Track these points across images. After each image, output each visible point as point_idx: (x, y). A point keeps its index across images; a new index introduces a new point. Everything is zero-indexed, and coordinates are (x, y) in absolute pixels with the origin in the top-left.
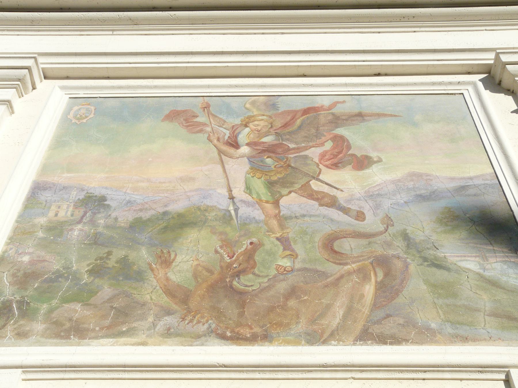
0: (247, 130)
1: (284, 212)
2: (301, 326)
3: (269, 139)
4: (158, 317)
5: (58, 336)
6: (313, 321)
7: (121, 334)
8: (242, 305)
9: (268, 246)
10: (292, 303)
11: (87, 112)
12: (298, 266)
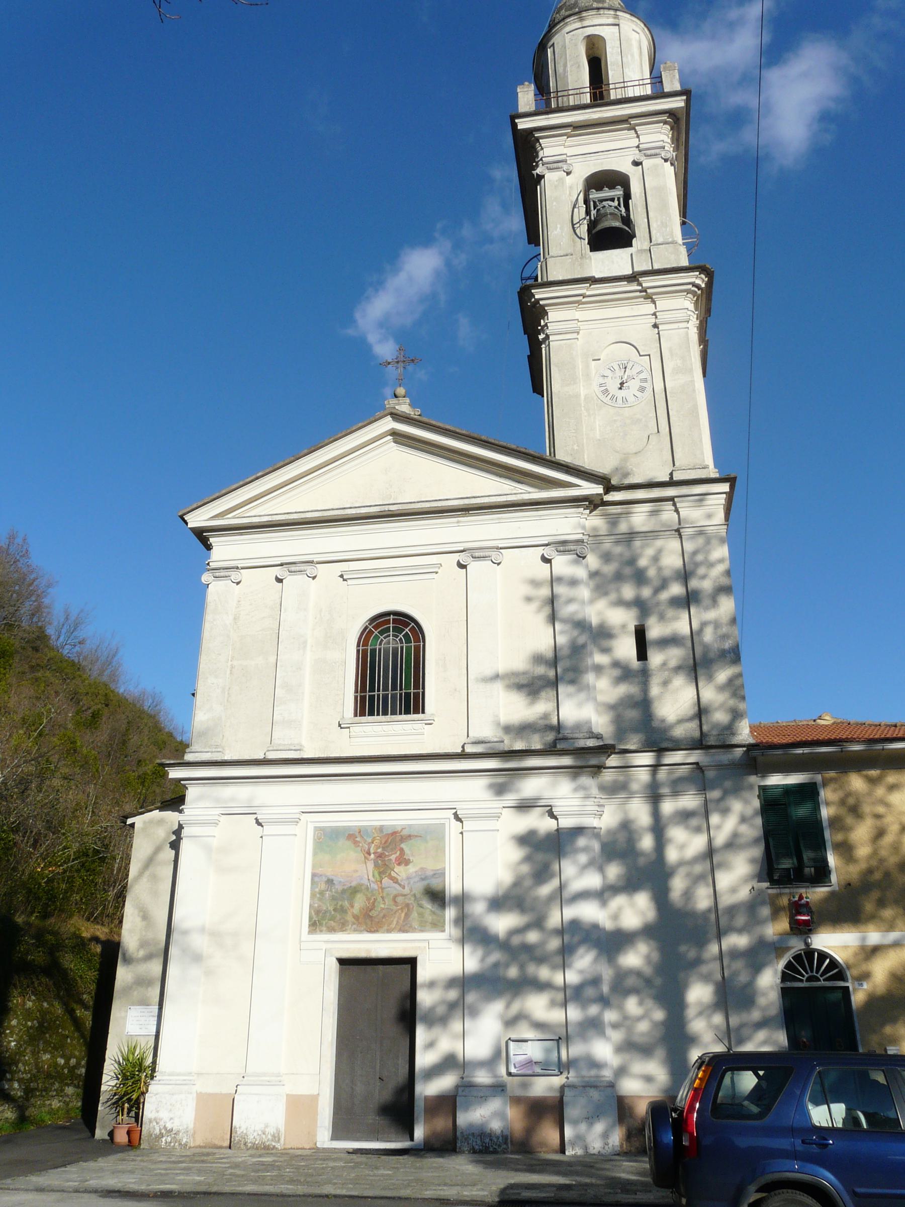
0: (373, 845)
1: (383, 886)
2: (385, 928)
3: (380, 850)
4: (352, 926)
5: (329, 931)
6: (388, 926)
7: (343, 931)
8: (372, 921)
9: (378, 900)
10: (384, 920)
11: (154, 704)
12: (386, 907)
